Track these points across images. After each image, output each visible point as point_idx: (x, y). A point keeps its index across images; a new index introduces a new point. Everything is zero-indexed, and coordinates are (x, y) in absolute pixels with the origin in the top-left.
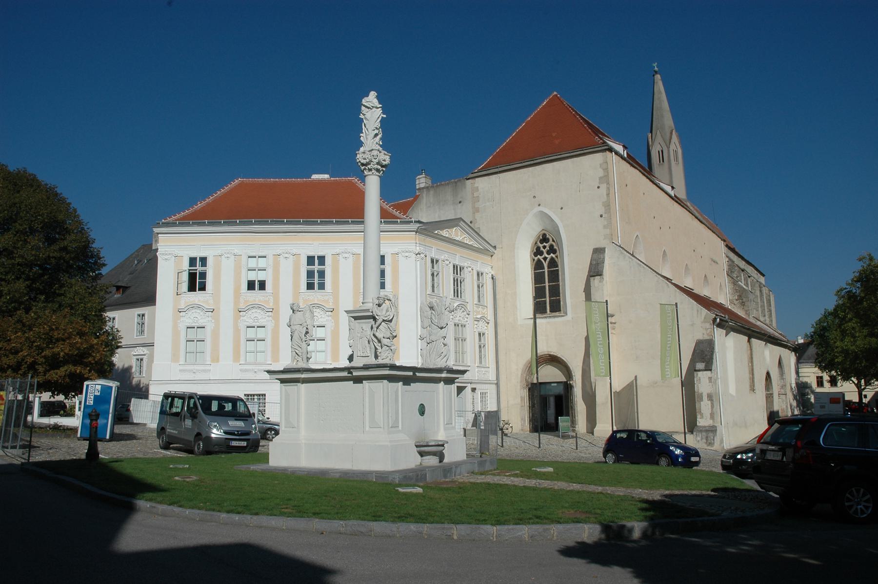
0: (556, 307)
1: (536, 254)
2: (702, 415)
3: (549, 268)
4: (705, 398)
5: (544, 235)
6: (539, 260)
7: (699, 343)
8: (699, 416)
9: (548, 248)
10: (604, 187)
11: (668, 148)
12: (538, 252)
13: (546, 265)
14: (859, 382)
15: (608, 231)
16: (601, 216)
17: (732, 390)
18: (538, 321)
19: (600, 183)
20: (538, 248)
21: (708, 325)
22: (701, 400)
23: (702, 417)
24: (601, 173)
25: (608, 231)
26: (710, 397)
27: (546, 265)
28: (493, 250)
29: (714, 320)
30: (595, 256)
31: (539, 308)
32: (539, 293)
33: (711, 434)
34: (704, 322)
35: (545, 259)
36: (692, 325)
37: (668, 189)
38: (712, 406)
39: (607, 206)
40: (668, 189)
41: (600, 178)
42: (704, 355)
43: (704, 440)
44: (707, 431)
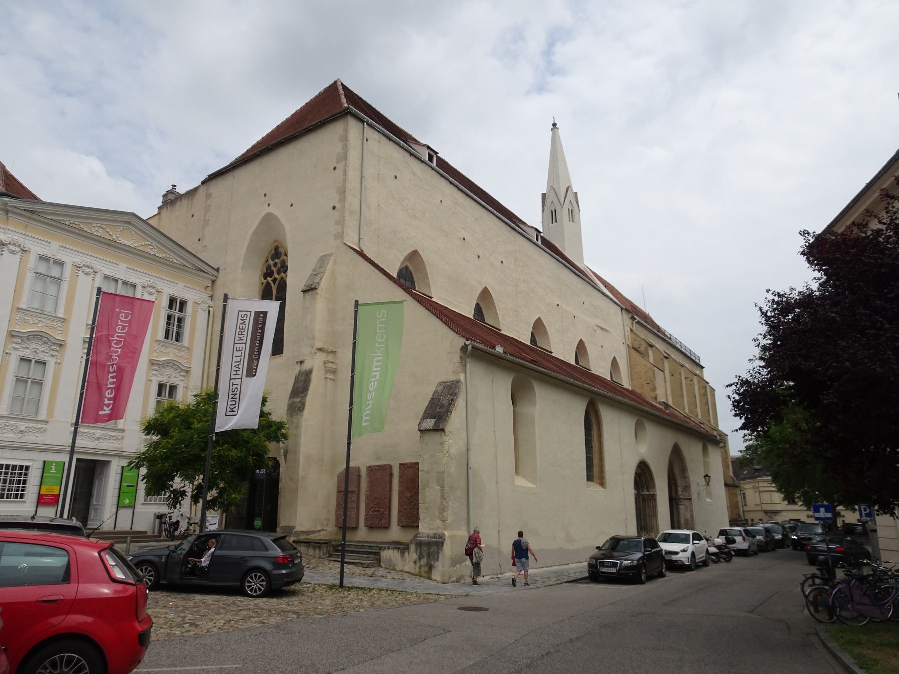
5: (277, 248)
6: (268, 283)
9: (279, 265)
12: (268, 273)
16: (334, 208)
28: (215, 273)
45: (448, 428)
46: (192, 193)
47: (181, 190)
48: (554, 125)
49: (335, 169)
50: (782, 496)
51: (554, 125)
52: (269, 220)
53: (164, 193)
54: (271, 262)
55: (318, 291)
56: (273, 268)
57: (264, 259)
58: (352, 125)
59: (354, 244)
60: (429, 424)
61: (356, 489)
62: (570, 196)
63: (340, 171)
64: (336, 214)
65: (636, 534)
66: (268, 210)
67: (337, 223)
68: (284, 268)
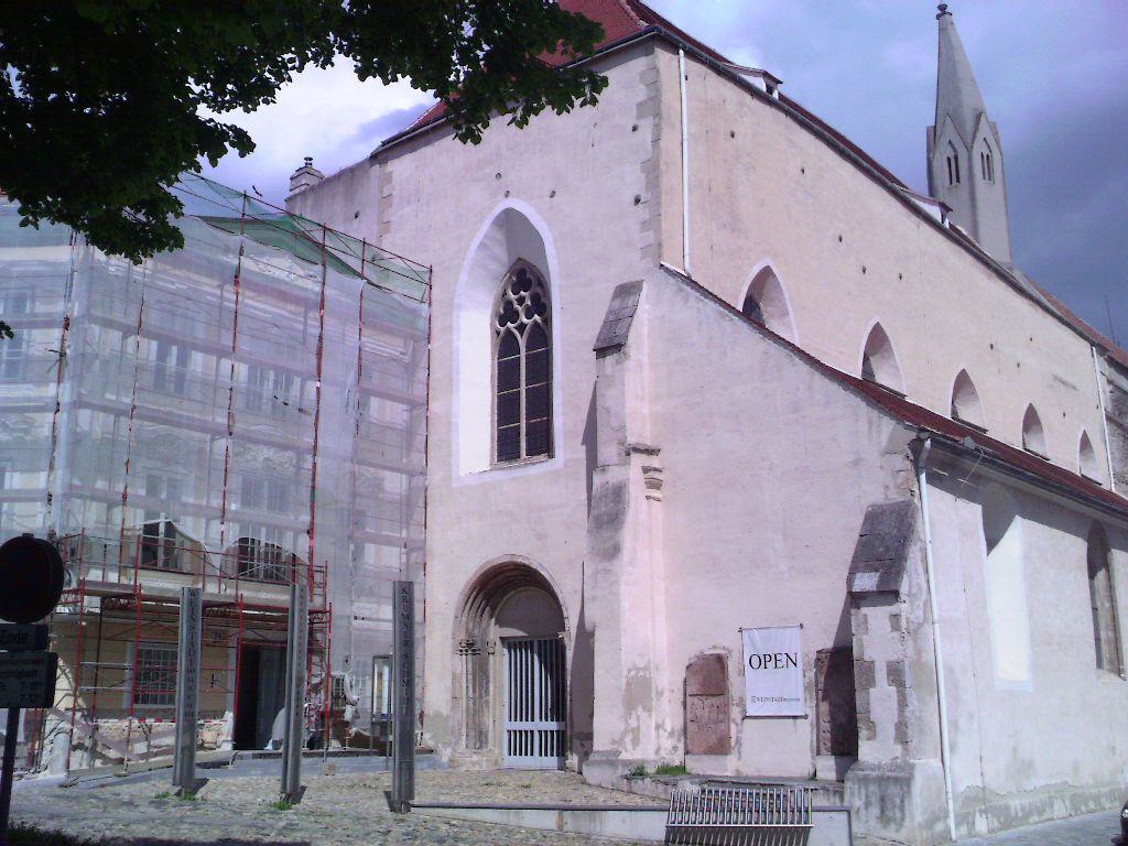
0: (542, 444)
1: (503, 320)
2: (872, 726)
3: (528, 348)
4: (881, 674)
6: (509, 331)
7: (873, 517)
8: (863, 733)
10: (646, 127)
11: (969, 149)
12: (507, 314)
13: (522, 342)
14: (65, 592)
15: (650, 237)
16: (637, 201)
17: (1012, 661)
18: (312, 441)
19: (640, 116)
20: (508, 304)
21: (901, 462)
22: (871, 682)
23: (871, 738)
24: (641, 93)
25: (650, 237)
26: (896, 673)
27: (522, 342)
29: (916, 446)
30: (617, 303)
31: (507, 449)
32: (506, 409)
33: (893, 790)
34: (888, 452)
35: (522, 328)
36: (856, 463)
37: (935, 212)
38: (903, 703)
39: (653, 170)
40: (935, 212)
41: (640, 105)
42: (884, 550)
43: (875, 811)
44: (881, 780)
45: (904, 589)
46: (350, 175)
47: (327, 166)
48: (943, 8)
49: (635, 129)
50: (532, 115)
51: (943, 8)
52: (511, 223)
53: (292, 172)
54: (513, 297)
55: (626, 349)
56: (516, 306)
57: (501, 291)
58: (662, 56)
59: (678, 265)
60: (867, 582)
61: (689, 724)
62: (984, 130)
63: (646, 132)
64: (642, 212)
65: (198, 762)
66: (502, 205)
67: (645, 225)
68: (541, 306)
